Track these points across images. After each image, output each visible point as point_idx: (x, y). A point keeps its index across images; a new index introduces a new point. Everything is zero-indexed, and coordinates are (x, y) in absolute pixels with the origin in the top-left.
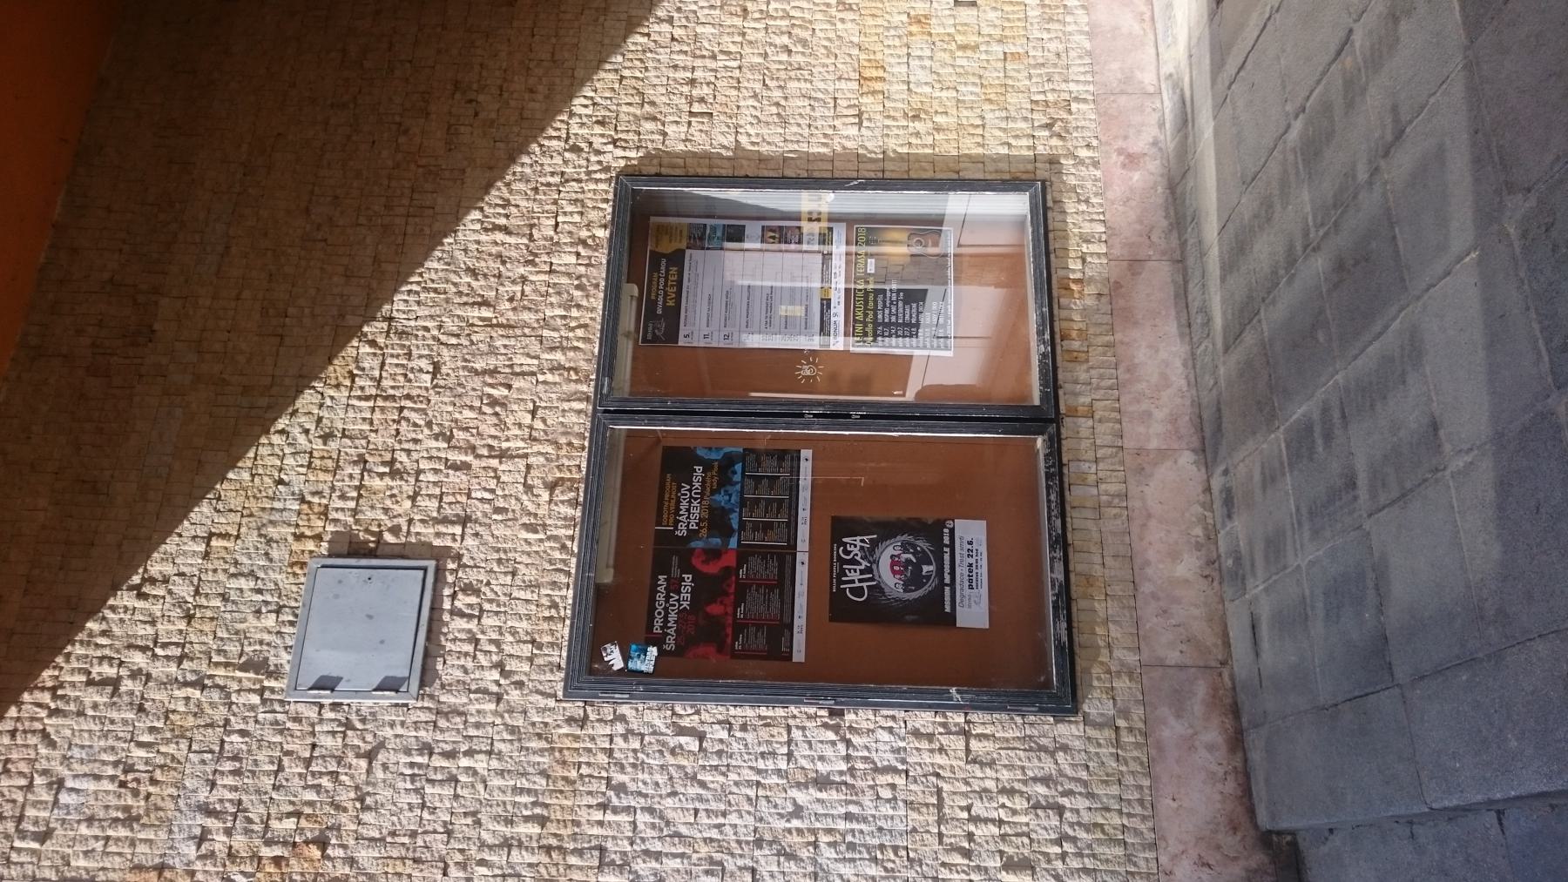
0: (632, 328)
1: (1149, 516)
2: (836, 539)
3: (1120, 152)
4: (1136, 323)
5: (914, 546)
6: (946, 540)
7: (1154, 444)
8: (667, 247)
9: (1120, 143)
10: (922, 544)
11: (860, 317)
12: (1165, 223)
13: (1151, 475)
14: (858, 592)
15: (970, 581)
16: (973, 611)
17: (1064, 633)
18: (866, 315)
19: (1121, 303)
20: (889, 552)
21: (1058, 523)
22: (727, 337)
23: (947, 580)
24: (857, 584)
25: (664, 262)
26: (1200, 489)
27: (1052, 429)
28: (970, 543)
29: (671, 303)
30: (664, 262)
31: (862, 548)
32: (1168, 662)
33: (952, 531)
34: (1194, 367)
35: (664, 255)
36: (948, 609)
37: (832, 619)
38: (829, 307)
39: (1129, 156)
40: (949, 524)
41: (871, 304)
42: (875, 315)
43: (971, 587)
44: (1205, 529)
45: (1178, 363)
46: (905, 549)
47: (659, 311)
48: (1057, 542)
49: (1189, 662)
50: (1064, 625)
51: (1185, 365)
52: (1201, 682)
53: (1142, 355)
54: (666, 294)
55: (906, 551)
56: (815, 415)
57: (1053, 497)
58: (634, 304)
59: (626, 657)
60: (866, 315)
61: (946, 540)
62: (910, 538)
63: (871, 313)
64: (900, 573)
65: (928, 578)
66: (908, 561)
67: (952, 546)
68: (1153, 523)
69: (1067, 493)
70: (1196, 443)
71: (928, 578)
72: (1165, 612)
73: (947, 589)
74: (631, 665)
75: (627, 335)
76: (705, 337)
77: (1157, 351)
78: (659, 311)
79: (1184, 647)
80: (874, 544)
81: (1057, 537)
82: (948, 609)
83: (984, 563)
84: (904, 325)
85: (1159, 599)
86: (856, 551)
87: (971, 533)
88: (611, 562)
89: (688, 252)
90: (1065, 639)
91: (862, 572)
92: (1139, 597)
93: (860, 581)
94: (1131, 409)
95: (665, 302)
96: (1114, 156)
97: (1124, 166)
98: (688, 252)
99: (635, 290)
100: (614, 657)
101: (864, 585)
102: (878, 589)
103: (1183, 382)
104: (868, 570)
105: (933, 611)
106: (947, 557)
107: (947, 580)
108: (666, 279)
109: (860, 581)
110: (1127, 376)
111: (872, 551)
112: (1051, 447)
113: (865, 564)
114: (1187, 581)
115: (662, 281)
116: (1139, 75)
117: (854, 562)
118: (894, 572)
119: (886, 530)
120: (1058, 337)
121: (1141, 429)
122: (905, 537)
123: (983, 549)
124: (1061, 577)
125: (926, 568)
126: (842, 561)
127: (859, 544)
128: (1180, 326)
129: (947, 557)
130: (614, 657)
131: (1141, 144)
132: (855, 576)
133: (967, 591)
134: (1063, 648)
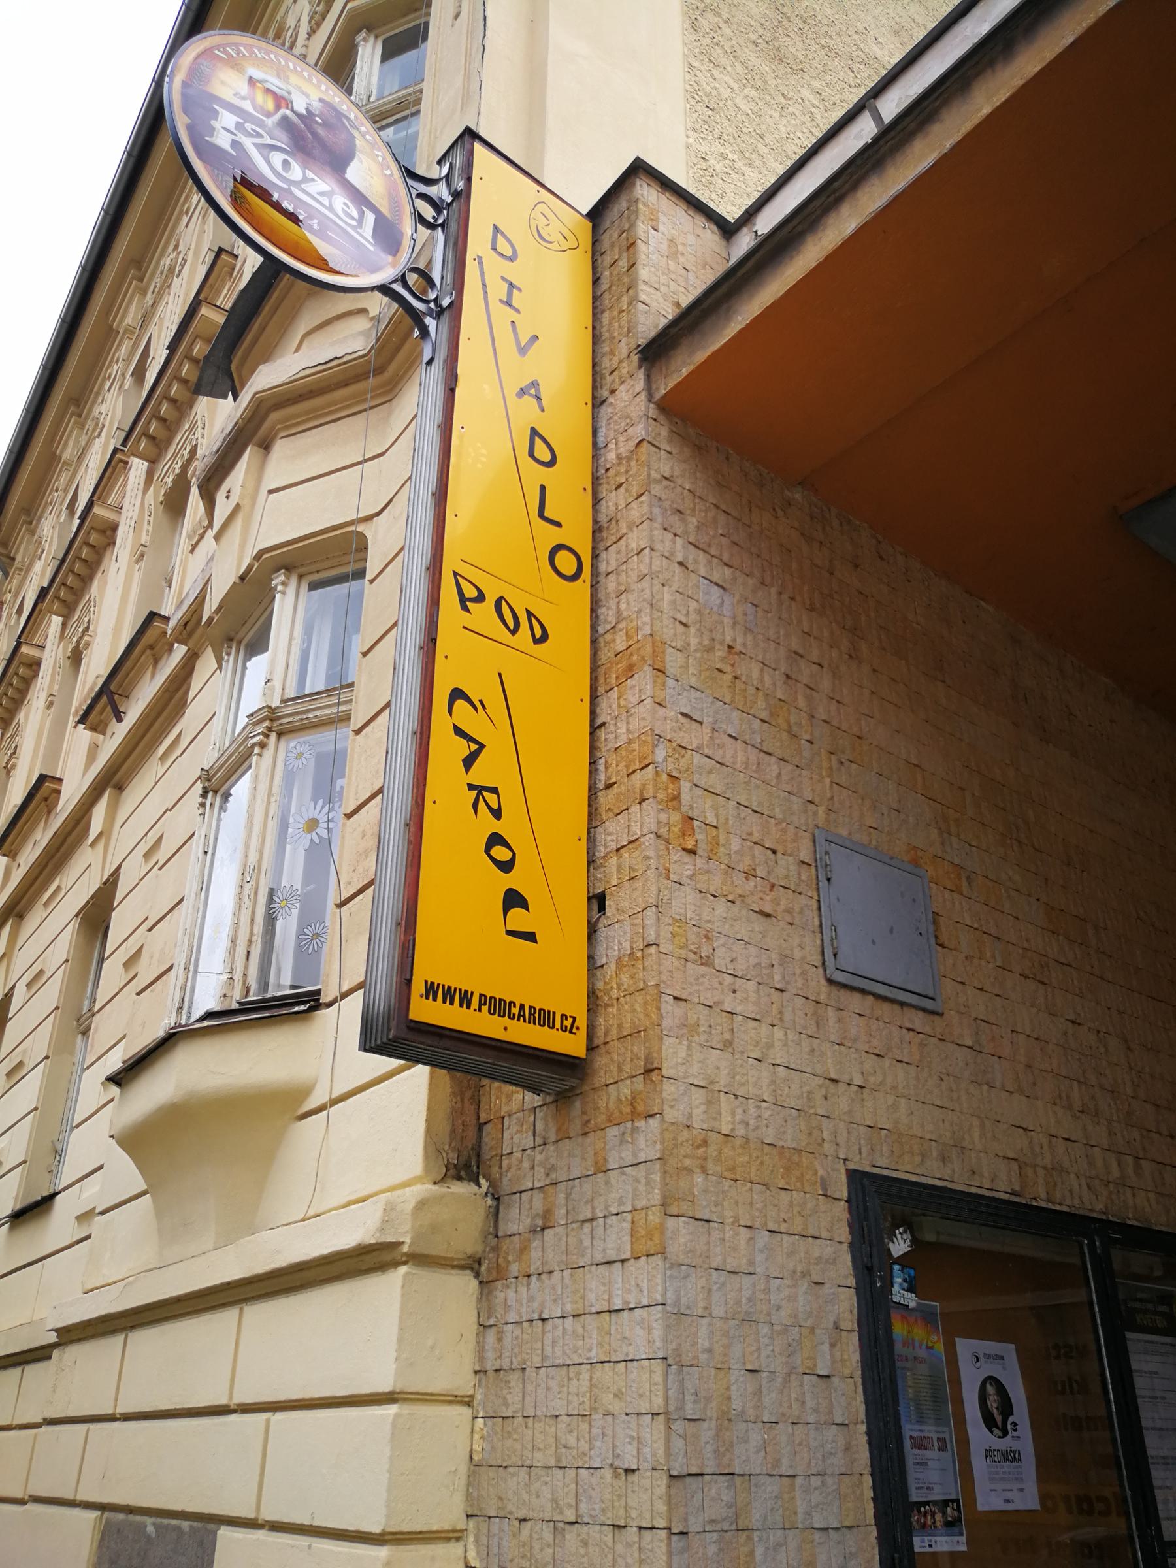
59: (903, 1260)
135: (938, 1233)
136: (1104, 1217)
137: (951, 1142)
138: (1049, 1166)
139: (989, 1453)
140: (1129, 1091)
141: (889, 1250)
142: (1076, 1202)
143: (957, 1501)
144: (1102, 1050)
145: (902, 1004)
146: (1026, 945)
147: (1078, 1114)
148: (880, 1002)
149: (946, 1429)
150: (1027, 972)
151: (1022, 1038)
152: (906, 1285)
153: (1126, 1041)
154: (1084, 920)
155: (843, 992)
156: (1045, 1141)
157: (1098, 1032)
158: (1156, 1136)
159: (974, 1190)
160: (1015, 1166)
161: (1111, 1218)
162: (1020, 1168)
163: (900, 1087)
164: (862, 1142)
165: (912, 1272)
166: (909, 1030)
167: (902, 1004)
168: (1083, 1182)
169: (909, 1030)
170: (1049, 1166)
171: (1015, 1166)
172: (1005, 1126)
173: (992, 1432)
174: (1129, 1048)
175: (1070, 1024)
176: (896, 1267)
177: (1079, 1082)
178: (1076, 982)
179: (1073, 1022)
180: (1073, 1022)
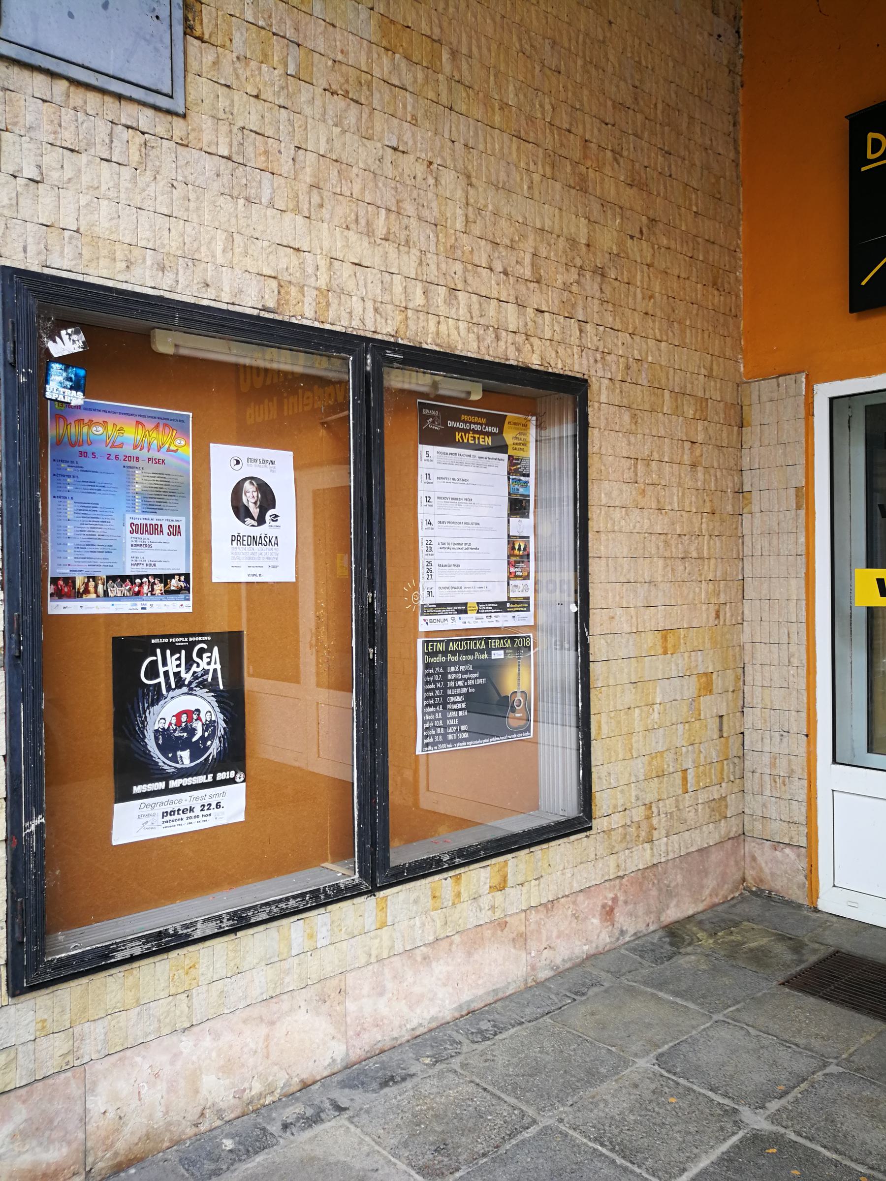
0: (442, 392)
1: (273, 1023)
2: (217, 639)
3: (615, 900)
4: (469, 954)
5: (212, 737)
6: (221, 776)
7: (351, 1006)
8: (509, 437)
9: (622, 898)
10: (214, 748)
11: (453, 647)
12: (558, 961)
13: (318, 1014)
14: (152, 671)
15: (172, 813)
16: (135, 822)
17: (127, 954)
18: (454, 653)
19: (488, 933)
20: (205, 705)
21: (263, 916)
22: (428, 499)
23: (173, 784)
24: (161, 670)
25: (496, 430)
26: (304, 1076)
27: (366, 886)
28: (218, 805)
29: (458, 437)
30: (496, 430)
31: (206, 672)
32: (89, 1098)
33: (232, 781)
34: (431, 1030)
35: (501, 432)
36: (137, 789)
37: (115, 639)
38: (460, 612)
39: (612, 910)
40: (240, 777)
41: (464, 658)
42: (454, 664)
43: (165, 814)
44: (261, 1096)
45: (433, 1011)
46: (210, 725)
47: (450, 424)
48: (241, 918)
49: (90, 1128)
50: (137, 951)
51: (433, 1019)
52: (65, 1150)
53: (440, 968)
54: (466, 431)
55: (206, 727)
56: (371, 605)
57: (292, 903)
58: (463, 396)
59: (67, 361)
60: (454, 653)
61: (221, 776)
62: (220, 732)
63: (455, 659)
64: (179, 723)
65: (174, 759)
66: (193, 732)
67: (215, 783)
68: (264, 1030)
69: (295, 918)
70: (353, 1057)
71: (174, 759)
72: (157, 1076)
73: (161, 785)
74: (56, 367)
75: (435, 385)
76: (428, 475)
77: (445, 985)
78: (450, 424)
79: (111, 1115)
80: (212, 687)
81: (247, 918)
82: (137, 789)
83: (196, 826)
84: (445, 696)
85: (172, 1063)
86: (203, 665)
87: (230, 803)
88: (183, 352)
89: (505, 457)
90: (119, 956)
91: (177, 675)
92: (174, 1038)
93: (166, 674)
94: (386, 971)
95: (460, 430)
96: (611, 895)
97: (604, 906)
98: (505, 457)
99: (476, 397)
100: (67, 344)
101: (161, 679)
102: (157, 696)
103: (414, 1023)
104: (180, 682)
105: (133, 771)
106: (201, 779)
107: (173, 784)
108: (480, 433)
109: (166, 674)
110: (419, 959)
111: (202, 685)
112: (347, 888)
113: (187, 677)
114: (197, 1092)
115: (478, 428)
116: (673, 903)
117: (190, 662)
118: (178, 716)
119: (232, 700)
120: (458, 871)
121: (366, 990)
122: (222, 725)
123: (211, 823)
124: (198, 934)
125: (185, 755)
126: (189, 648)
127: (211, 668)
128: (469, 1002)
129: (201, 779)
130: (67, 344)
131: (621, 919)
132: (172, 667)
133: (159, 811)
134: (107, 957)
135: (176, 346)
136: (392, 340)
137: (179, 253)
138: (324, 287)
139: (236, 539)
140: (459, 225)
141: (47, 349)
142: (355, 324)
143: (187, 576)
144: (431, 181)
145: (120, 97)
146: (339, 57)
147: (379, 241)
148: (160, 114)
149: (183, 519)
150: (334, 87)
151: (311, 158)
152: (69, 384)
153: (469, 177)
154: (439, 41)
155: (16, 69)
156: (323, 263)
157: (431, 163)
158: (485, 272)
159: (205, 303)
160: (274, 284)
161: (400, 341)
162: (280, 286)
163: (104, 187)
164: (30, 240)
165: (82, 373)
166: (128, 127)
167: (120, 97)
168: (370, 305)
169: (128, 127)
170: (324, 287)
171: (274, 284)
172: (266, 244)
173: (244, 522)
174: (470, 184)
175: (390, 151)
176: (56, 367)
177: (388, 210)
178: (409, 108)
179: (395, 149)
180: (395, 149)
